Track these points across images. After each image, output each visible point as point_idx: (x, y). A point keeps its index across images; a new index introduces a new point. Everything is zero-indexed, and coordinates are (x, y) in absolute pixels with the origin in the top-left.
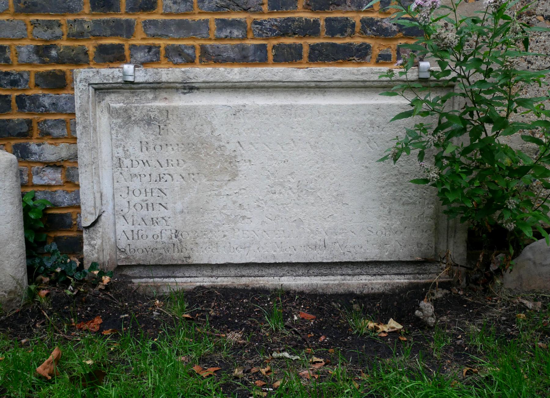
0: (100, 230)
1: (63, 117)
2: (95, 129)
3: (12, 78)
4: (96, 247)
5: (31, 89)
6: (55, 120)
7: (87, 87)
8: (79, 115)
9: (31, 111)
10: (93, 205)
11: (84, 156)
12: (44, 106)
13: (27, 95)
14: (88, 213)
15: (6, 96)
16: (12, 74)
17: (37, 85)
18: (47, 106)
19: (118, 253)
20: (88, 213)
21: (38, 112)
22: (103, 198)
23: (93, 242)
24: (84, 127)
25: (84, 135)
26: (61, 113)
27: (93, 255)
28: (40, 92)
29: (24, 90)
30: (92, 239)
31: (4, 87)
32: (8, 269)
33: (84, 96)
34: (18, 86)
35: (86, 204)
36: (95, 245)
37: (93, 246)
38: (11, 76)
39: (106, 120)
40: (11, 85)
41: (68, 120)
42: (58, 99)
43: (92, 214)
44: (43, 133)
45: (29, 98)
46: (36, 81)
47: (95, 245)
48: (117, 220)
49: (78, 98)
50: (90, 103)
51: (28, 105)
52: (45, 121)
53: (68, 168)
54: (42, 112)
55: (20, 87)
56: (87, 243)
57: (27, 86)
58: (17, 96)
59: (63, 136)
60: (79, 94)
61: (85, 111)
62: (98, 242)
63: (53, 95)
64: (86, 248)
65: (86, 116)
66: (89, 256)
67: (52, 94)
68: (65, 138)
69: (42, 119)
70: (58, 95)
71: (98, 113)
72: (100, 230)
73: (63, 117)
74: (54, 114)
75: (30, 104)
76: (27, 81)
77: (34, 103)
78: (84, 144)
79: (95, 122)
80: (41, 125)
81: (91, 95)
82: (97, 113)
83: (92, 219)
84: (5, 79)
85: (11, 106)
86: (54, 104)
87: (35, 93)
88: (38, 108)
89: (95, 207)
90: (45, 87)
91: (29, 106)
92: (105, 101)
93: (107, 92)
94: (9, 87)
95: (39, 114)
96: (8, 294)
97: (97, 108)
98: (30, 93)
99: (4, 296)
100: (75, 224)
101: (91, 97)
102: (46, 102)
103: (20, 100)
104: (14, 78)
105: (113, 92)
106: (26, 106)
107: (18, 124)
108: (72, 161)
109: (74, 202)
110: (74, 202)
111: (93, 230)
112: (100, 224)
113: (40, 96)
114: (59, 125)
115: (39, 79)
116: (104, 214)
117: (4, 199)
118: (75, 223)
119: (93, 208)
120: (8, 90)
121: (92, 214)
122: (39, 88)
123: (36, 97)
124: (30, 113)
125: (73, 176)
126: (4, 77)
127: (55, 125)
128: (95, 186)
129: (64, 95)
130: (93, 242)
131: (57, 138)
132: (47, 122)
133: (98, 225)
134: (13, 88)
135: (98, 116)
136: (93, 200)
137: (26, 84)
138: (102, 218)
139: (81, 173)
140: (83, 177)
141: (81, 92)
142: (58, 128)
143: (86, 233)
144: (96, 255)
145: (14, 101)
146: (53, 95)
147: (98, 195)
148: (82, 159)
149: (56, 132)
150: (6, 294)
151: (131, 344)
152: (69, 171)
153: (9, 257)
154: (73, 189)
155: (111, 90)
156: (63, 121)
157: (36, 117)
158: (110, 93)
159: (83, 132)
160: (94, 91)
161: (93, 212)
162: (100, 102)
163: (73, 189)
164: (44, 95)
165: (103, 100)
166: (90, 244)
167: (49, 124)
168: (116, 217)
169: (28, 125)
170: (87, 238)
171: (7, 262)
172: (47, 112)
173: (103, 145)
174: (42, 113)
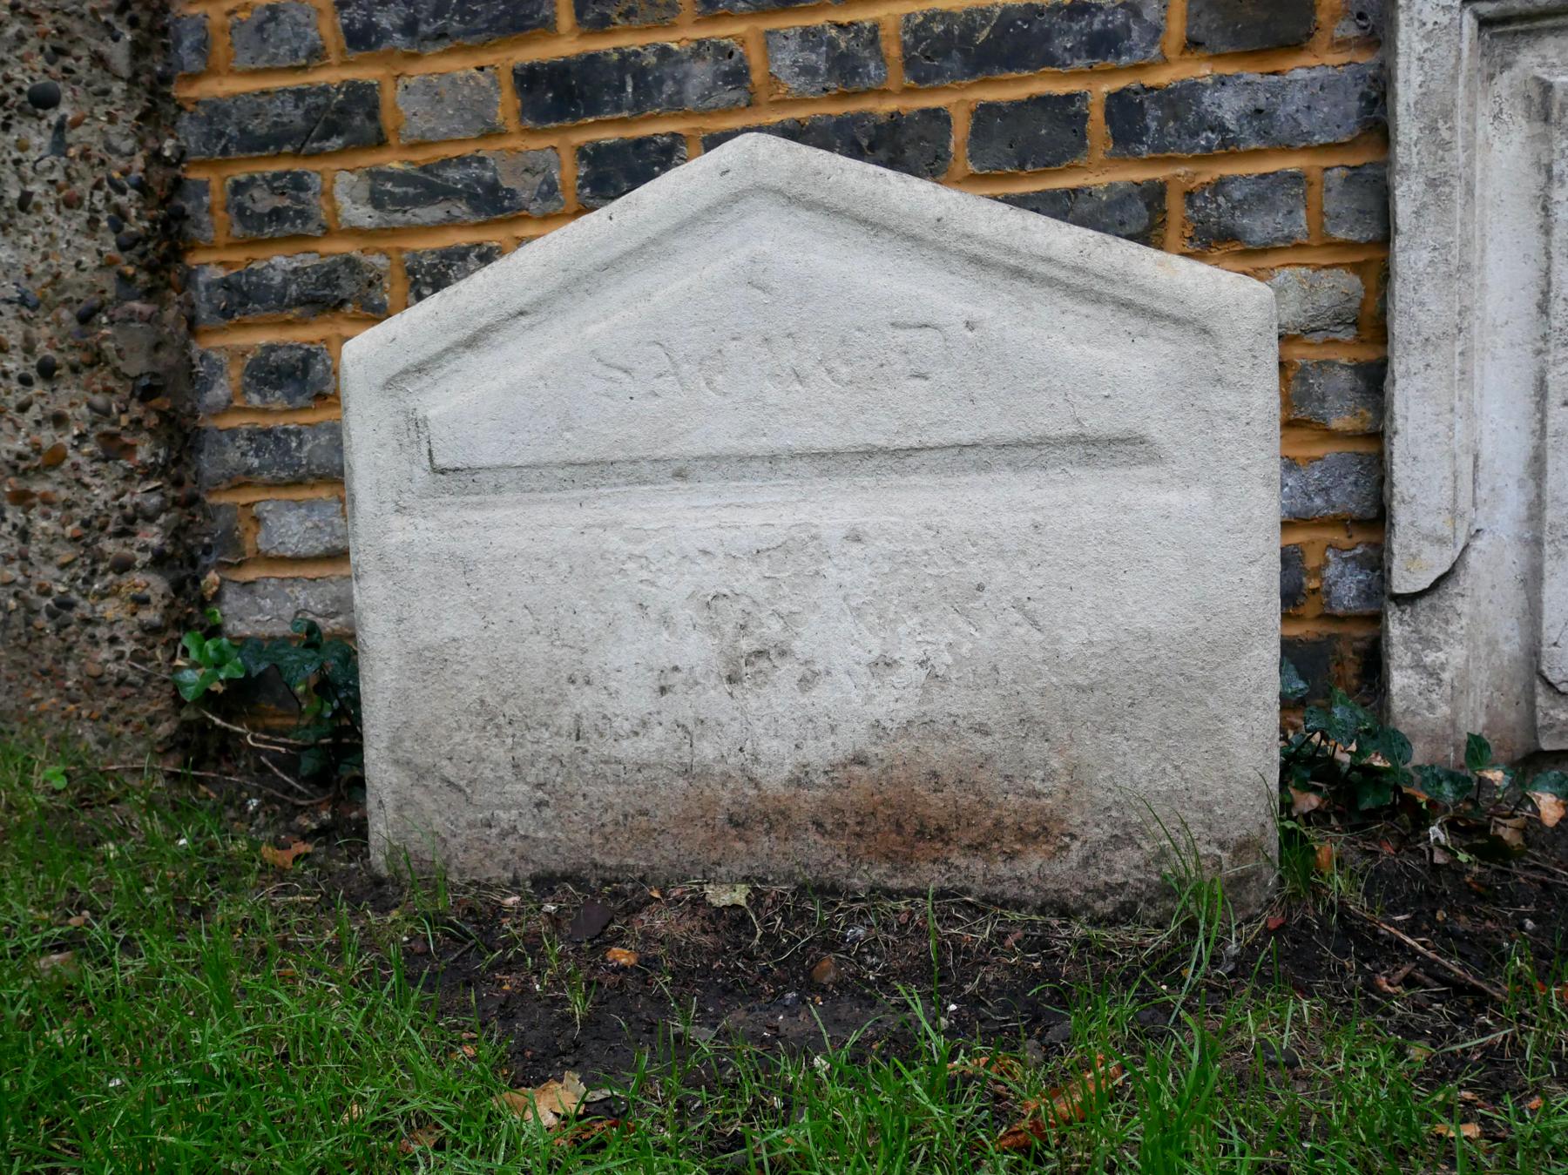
0: (1463, 606)
1: (1293, 164)
2: (1470, 191)
3: (1097, 25)
4: (1446, 676)
5: (1166, 61)
6: (1264, 176)
7: (1455, 13)
8: (1415, 134)
9: (1166, 149)
10: (1447, 504)
11: (1422, 304)
12: (1220, 128)
13: (1152, 89)
14: (1426, 537)
15: (1070, 98)
16: (1100, 8)
17: (1193, 45)
18: (1231, 123)
19: (1541, 700)
20: (1426, 537)
21: (1193, 149)
22: (1482, 476)
23: (1430, 657)
24: (1432, 184)
25: (1431, 215)
26: (1287, 149)
27: (1431, 707)
28: (1203, 71)
29: (1138, 68)
30: (1429, 642)
31: (1065, 65)
32: (1244, 753)
33: (1442, 50)
34: (1118, 55)
35: (1420, 499)
36: (1443, 667)
37: (1433, 673)
38: (1094, 15)
39: (1514, 149)
40: (1092, 54)
41: (1315, 175)
42: (1277, 92)
43: (1441, 541)
44: (1207, 233)
45: (1157, 100)
46: (1190, 28)
47: (1443, 667)
48: (1548, 566)
49: (1415, 64)
50: (1461, 80)
51: (1153, 125)
52: (1219, 186)
53: (1303, 369)
54: (1208, 149)
55: (1125, 59)
56: (1407, 660)
57: (1155, 51)
58: (1112, 96)
59: (1288, 238)
60: (1419, 48)
61: (1437, 117)
62: (1452, 656)
63: (1258, 79)
64: (1401, 680)
65: (1446, 135)
66: (1414, 714)
67: (1251, 73)
68: (1299, 246)
69: (1207, 179)
70: (1276, 78)
71: (1484, 124)
72: (1463, 606)
73: (1293, 164)
74: (1256, 151)
75: (1162, 123)
76: (1156, 32)
77: (1176, 118)
78: (1426, 255)
79: (1470, 163)
80: (1198, 203)
81: (1465, 46)
82: (1480, 122)
83: (1436, 562)
84: (1066, 33)
85: (1084, 137)
86: (1259, 111)
87: (1183, 76)
88: (1194, 134)
89: (1454, 513)
90: (1224, 49)
91: (1160, 131)
92: (1516, 70)
93: (1527, 33)
94: (1080, 64)
95: (1197, 159)
96: (1235, 853)
97: (1480, 103)
98: (1162, 78)
99: (1218, 863)
100: (1314, 591)
101: (1466, 53)
102: (1229, 106)
103: (1123, 110)
104: (1105, 23)
105: (1553, 30)
106: (1147, 128)
107: (1109, 205)
108: (1317, 337)
109: (1318, 501)
110: (1318, 501)
111: (1433, 607)
112: (1465, 581)
113: (1205, 87)
114: (1279, 195)
115: (1205, 18)
116: (1479, 544)
117: (1243, 461)
118: (1314, 584)
119: (1446, 516)
120: (1078, 74)
121: (1441, 541)
122: (1201, 52)
123: (1191, 90)
124: (1162, 156)
125: (1322, 399)
126: (1064, 25)
127: (1261, 198)
128: (1458, 427)
129: (1300, 74)
130: (1430, 657)
131: (1265, 250)
132: (1229, 188)
133: (1452, 588)
134: (1099, 63)
135: (1480, 135)
136: (1449, 483)
137: (1153, 43)
138: (1472, 558)
139: (1407, 373)
140: (1411, 392)
141: (1427, 37)
142: (1273, 208)
143: (1401, 622)
144: (1444, 710)
145: (1097, 114)
146: (1258, 79)
147: (1466, 463)
148: (1412, 318)
149: (1259, 226)
150: (1225, 856)
151: (434, 937)
152: (1304, 379)
153: (1248, 702)
154: (1317, 451)
155: (1549, 23)
156: (1297, 178)
157: (1181, 170)
158: (1538, 34)
159: (1424, 206)
160: (1476, 25)
161: (1447, 532)
162: (1491, 77)
163: (1317, 451)
164: (1222, 82)
165: (1507, 66)
166: (1418, 666)
167: (1237, 195)
168: (1548, 549)
169: (1149, 206)
170: (1406, 642)
171: (1238, 722)
172: (1229, 148)
173: (1492, 257)
174: (1208, 156)
